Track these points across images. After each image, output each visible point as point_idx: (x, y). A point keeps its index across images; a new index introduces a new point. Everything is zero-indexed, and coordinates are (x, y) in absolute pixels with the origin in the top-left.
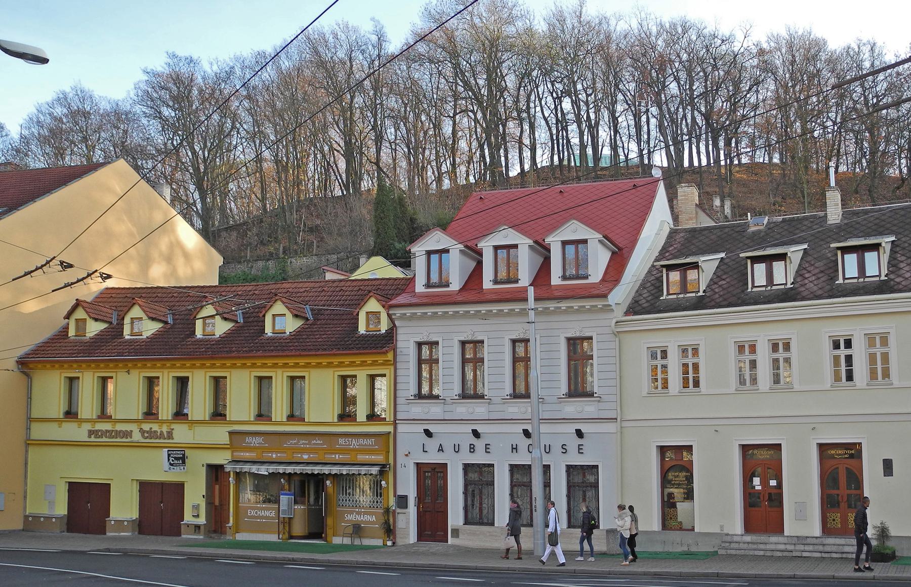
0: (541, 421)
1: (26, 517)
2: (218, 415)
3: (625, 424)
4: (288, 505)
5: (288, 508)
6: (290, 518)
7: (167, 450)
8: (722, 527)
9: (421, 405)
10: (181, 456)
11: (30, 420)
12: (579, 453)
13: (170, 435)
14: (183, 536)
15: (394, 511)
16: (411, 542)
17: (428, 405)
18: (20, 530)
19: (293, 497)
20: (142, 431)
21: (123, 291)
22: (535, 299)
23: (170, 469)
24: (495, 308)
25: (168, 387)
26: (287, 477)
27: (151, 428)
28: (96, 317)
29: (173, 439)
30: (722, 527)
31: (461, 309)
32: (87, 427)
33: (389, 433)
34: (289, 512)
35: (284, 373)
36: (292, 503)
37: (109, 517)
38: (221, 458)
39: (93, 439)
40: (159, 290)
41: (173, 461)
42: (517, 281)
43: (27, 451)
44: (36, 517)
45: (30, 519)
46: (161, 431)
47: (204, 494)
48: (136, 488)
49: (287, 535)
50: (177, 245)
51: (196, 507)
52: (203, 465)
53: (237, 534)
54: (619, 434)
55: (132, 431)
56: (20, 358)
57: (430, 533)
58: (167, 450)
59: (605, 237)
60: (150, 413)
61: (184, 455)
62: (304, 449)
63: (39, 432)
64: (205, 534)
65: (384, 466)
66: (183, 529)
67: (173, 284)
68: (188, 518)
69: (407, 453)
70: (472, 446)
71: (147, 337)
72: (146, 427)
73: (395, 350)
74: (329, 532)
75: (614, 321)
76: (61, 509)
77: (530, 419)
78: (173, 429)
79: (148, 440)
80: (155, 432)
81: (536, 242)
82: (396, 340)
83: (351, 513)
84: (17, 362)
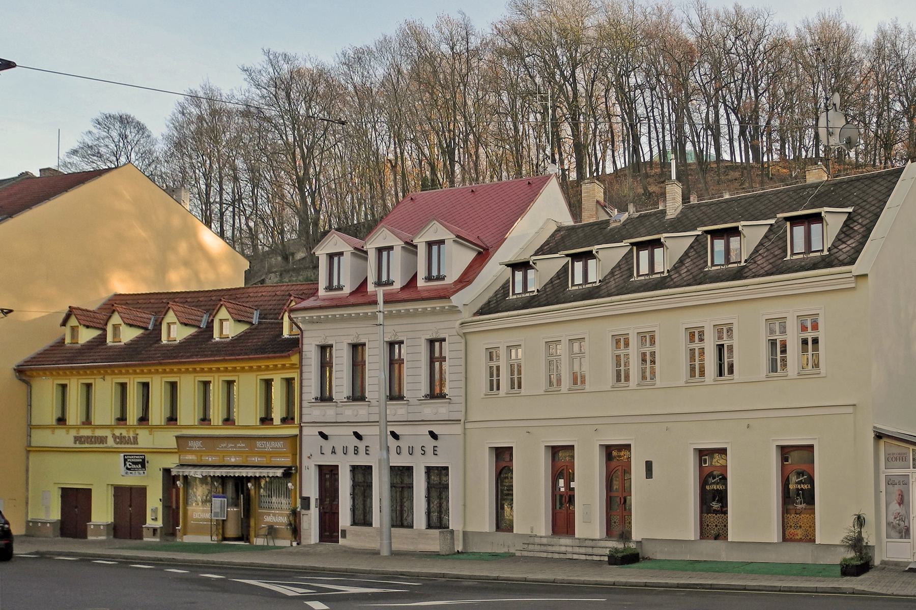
0: (388, 423)
1: (28, 522)
2: (172, 419)
3: (468, 426)
4: (221, 507)
5: (221, 511)
6: (223, 520)
7: (122, 455)
8: (532, 529)
9: (351, 407)
10: (141, 460)
11: (31, 427)
12: (434, 454)
13: (135, 439)
14: (145, 539)
15: (300, 512)
16: (313, 542)
17: (324, 408)
18: (21, 536)
19: (226, 500)
20: (114, 436)
21: (135, 297)
22: (384, 302)
23: (127, 473)
24: (429, 305)
25: (134, 392)
26: (220, 481)
27: (121, 434)
28: (87, 324)
29: (137, 444)
30: (532, 529)
31: (353, 311)
32: (73, 433)
33: (297, 435)
34: (221, 514)
35: (220, 377)
36: (224, 507)
37: (90, 521)
38: (171, 462)
39: (78, 445)
40: (200, 294)
41: (130, 465)
42: (392, 284)
43: (28, 458)
44: (35, 523)
45: (31, 524)
46: (129, 437)
47: (161, 498)
48: (111, 492)
49: (220, 537)
50: (200, 248)
51: (155, 511)
52: (160, 470)
53: (184, 537)
54: (462, 435)
55: (107, 437)
56: (18, 366)
57: (328, 534)
58: (122, 455)
59: (458, 236)
60: (122, 419)
61: (144, 460)
62: (232, 452)
63: (40, 438)
64: (161, 537)
65: (290, 468)
66: (145, 531)
67: (194, 288)
68: (150, 523)
69: (309, 455)
70: (356, 448)
71: (125, 344)
72: (117, 432)
73: (300, 352)
74: (252, 533)
75: (460, 322)
76: (55, 515)
77: (378, 422)
78: (138, 434)
79: (119, 446)
80: (124, 437)
81: (406, 243)
82: (302, 344)
83: (269, 514)
84: (15, 370)
